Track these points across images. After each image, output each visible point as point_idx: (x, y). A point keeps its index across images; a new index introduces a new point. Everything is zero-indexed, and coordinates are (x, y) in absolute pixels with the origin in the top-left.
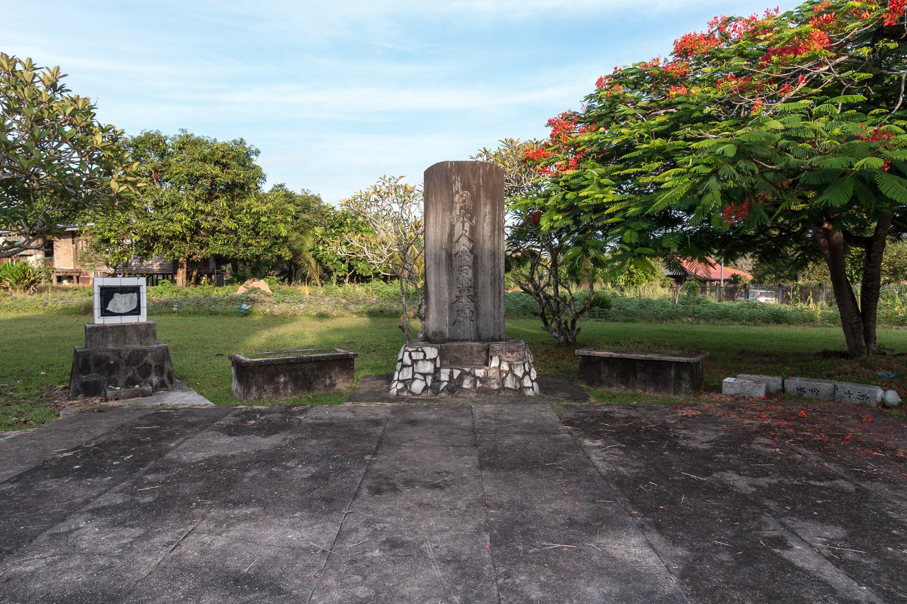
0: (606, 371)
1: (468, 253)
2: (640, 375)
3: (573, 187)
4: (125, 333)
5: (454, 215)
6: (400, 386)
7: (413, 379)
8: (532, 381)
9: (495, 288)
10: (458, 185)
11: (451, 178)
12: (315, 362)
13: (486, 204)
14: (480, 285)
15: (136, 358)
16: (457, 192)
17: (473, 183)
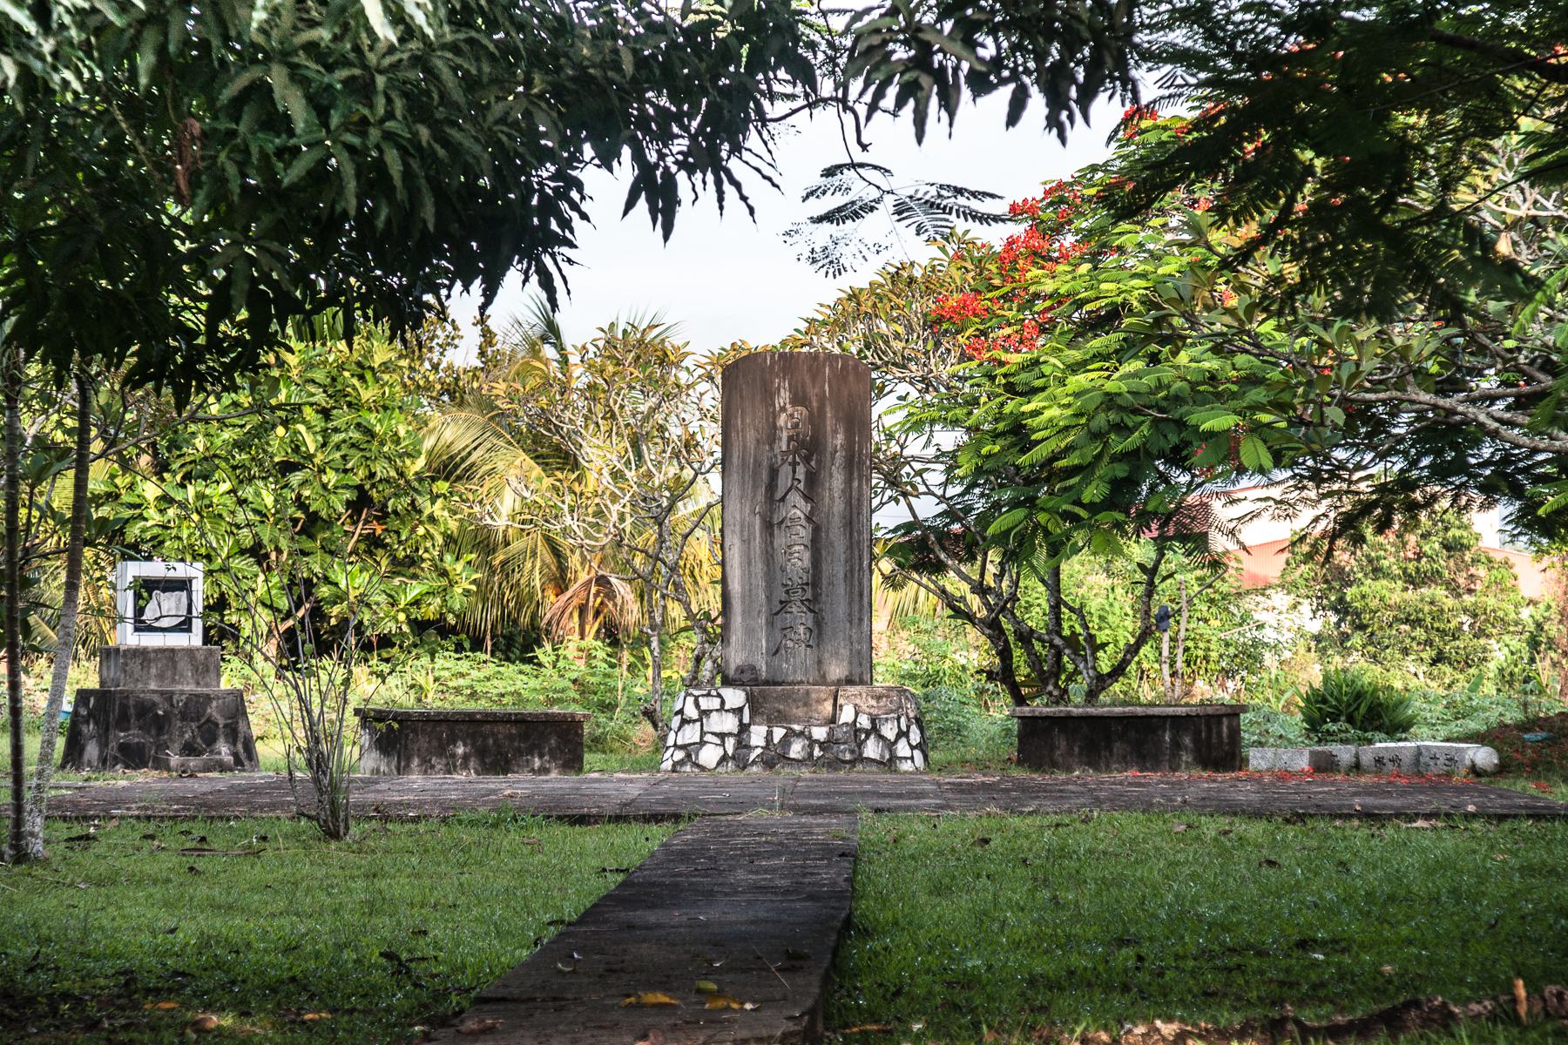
0: (1062, 743)
1: (803, 522)
2: (1118, 747)
3: (1020, 389)
4: (174, 663)
5: (777, 451)
6: (680, 755)
7: (702, 743)
8: (912, 748)
9: (852, 585)
10: (783, 398)
11: (772, 382)
12: (516, 722)
13: (835, 432)
14: (825, 582)
15: (195, 708)
16: (783, 409)
17: (812, 392)
